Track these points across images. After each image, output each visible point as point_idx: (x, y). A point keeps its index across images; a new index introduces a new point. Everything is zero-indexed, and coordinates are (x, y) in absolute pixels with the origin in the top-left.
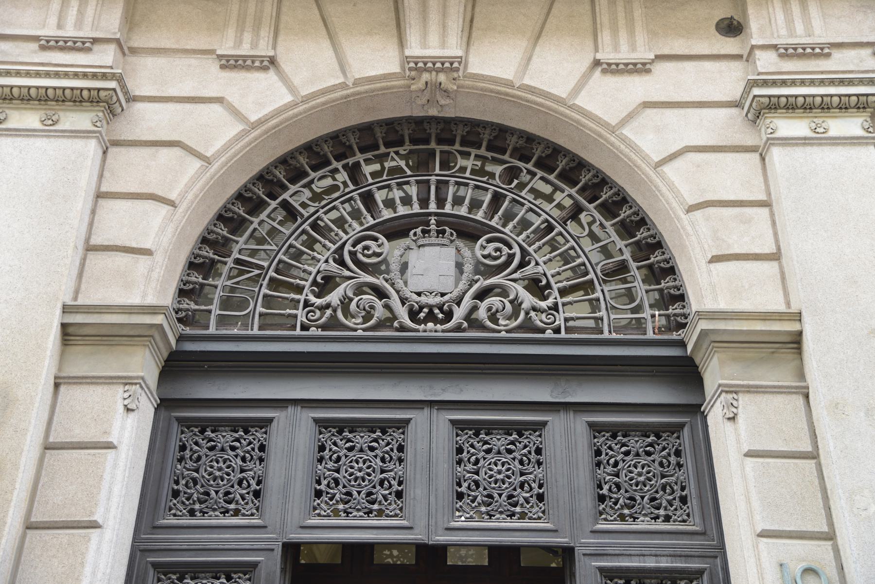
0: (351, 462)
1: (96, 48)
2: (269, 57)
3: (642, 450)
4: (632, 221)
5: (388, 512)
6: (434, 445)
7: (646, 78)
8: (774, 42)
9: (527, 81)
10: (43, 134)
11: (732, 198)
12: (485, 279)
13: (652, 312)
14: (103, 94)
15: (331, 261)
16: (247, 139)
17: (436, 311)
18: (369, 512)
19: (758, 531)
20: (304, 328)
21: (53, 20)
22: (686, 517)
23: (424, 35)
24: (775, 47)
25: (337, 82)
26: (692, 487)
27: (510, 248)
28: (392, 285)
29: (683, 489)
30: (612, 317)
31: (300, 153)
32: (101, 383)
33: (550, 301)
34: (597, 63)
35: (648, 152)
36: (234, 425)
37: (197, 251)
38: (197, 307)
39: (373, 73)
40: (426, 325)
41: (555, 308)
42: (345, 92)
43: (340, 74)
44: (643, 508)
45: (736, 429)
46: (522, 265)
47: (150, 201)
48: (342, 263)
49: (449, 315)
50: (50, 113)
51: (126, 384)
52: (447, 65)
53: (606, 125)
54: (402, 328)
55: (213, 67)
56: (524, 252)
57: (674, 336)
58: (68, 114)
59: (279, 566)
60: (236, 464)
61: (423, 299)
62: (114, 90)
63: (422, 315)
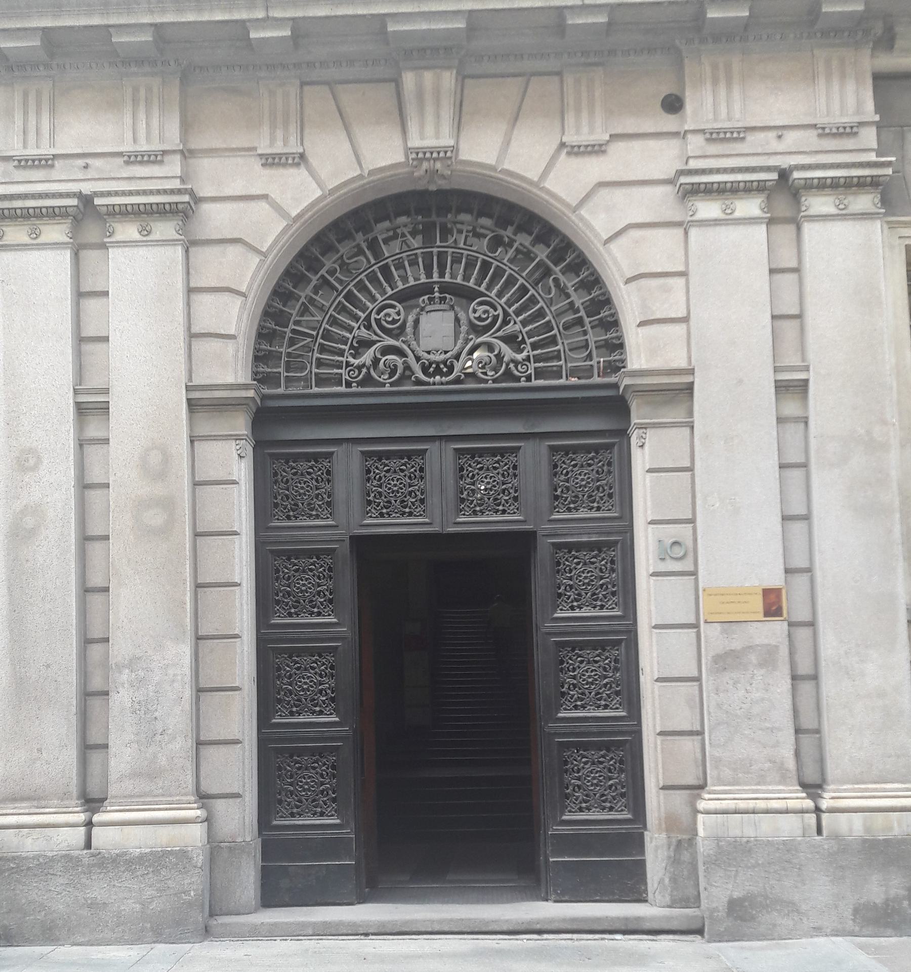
0: (389, 480)
1: (167, 158)
2: (300, 154)
3: (585, 463)
4: (588, 281)
5: (415, 513)
6: (444, 467)
7: (602, 158)
8: (703, 127)
9: (506, 166)
10: (143, 244)
11: (659, 270)
12: (477, 337)
13: (598, 359)
14: (180, 207)
15: (362, 328)
16: (290, 232)
17: (442, 366)
18: (403, 514)
19: (649, 520)
20: (349, 384)
21: (129, 135)
22: (610, 507)
23: (422, 126)
24: (703, 131)
25: (355, 175)
26: (617, 487)
27: (496, 310)
28: (409, 346)
29: (611, 488)
30: (569, 365)
31: (330, 230)
32: (220, 440)
33: (525, 354)
34: (563, 145)
35: (599, 231)
36: (308, 457)
37: (262, 323)
38: (269, 370)
39: (383, 164)
40: (434, 378)
41: (528, 359)
42: (362, 182)
43: (356, 166)
44: (583, 503)
45: (643, 453)
46: (505, 322)
47: (227, 293)
48: (369, 327)
49: (451, 369)
50: (144, 224)
51: (237, 439)
52: (442, 154)
53: (568, 205)
54: (419, 382)
55: (256, 164)
56: (506, 314)
57: (612, 379)
58: (156, 223)
59: (349, 550)
60: (312, 484)
61: (432, 357)
62: (189, 203)
63: (431, 370)
